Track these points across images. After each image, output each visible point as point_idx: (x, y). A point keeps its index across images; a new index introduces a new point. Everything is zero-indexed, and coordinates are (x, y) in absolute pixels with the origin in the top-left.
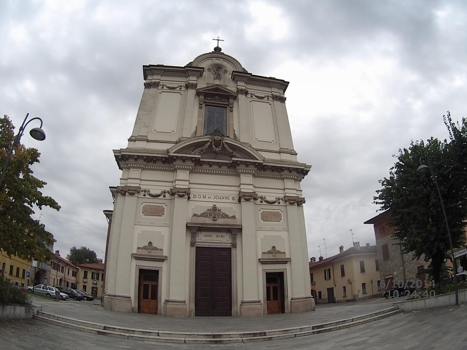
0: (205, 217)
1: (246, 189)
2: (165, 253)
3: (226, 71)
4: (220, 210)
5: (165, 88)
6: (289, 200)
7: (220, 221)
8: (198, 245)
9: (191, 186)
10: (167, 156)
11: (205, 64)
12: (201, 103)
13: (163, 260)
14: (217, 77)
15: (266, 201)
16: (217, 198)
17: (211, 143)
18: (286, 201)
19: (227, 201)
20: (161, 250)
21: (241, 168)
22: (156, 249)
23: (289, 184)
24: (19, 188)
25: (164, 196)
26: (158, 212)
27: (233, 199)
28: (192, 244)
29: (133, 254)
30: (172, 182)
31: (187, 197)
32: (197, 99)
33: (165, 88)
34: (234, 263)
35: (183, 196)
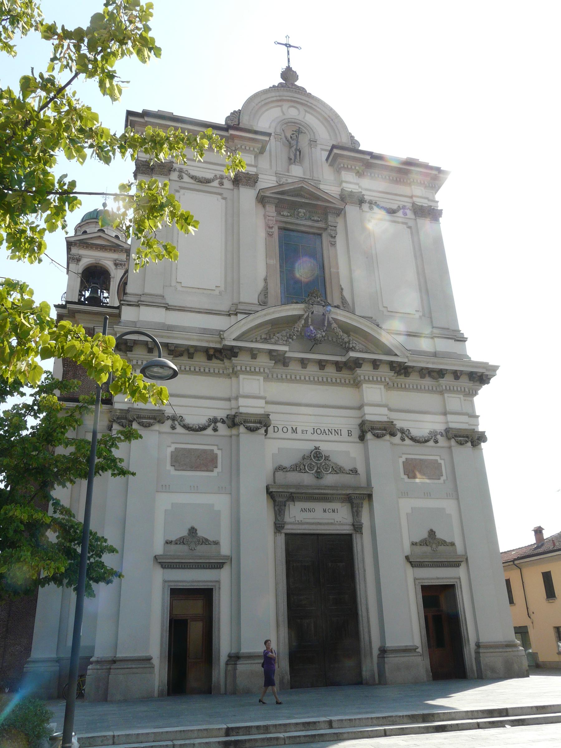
0: (300, 471)
1: (375, 414)
2: (225, 549)
3: (313, 142)
4: (327, 458)
5: (186, 179)
6: (456, 436)
7: (330, 479)
8: (289, 529)
9: (270, 408)
10: (218, 346)
11: (266, 122)
12: (271, 223)
13: (219, 566)
14: (295, 155)
15: (413, 439)
16: (319, 431)
17: (306, 320)
18: (449, 439)
19: (337, 438)
20: (217, 543)
21: (365, 371)
22: (205, 541)
23: (454, 402)
24: (56, 420)
25: (215, 430)
26: (204, 461)
27: (350, 433)
28: (278, 527)
29: (156, 558)
30: (229, 400)
31: (262, 431)
32: (261, 211)
33: (186, 179)
34: (361, 566)
35: (257, 429)
